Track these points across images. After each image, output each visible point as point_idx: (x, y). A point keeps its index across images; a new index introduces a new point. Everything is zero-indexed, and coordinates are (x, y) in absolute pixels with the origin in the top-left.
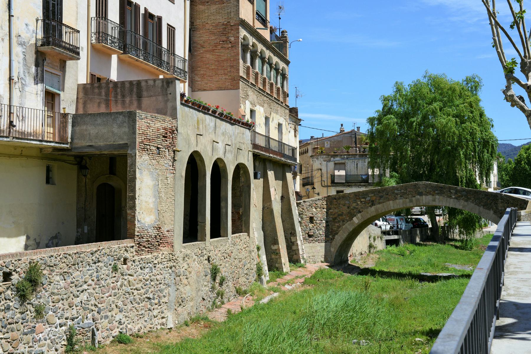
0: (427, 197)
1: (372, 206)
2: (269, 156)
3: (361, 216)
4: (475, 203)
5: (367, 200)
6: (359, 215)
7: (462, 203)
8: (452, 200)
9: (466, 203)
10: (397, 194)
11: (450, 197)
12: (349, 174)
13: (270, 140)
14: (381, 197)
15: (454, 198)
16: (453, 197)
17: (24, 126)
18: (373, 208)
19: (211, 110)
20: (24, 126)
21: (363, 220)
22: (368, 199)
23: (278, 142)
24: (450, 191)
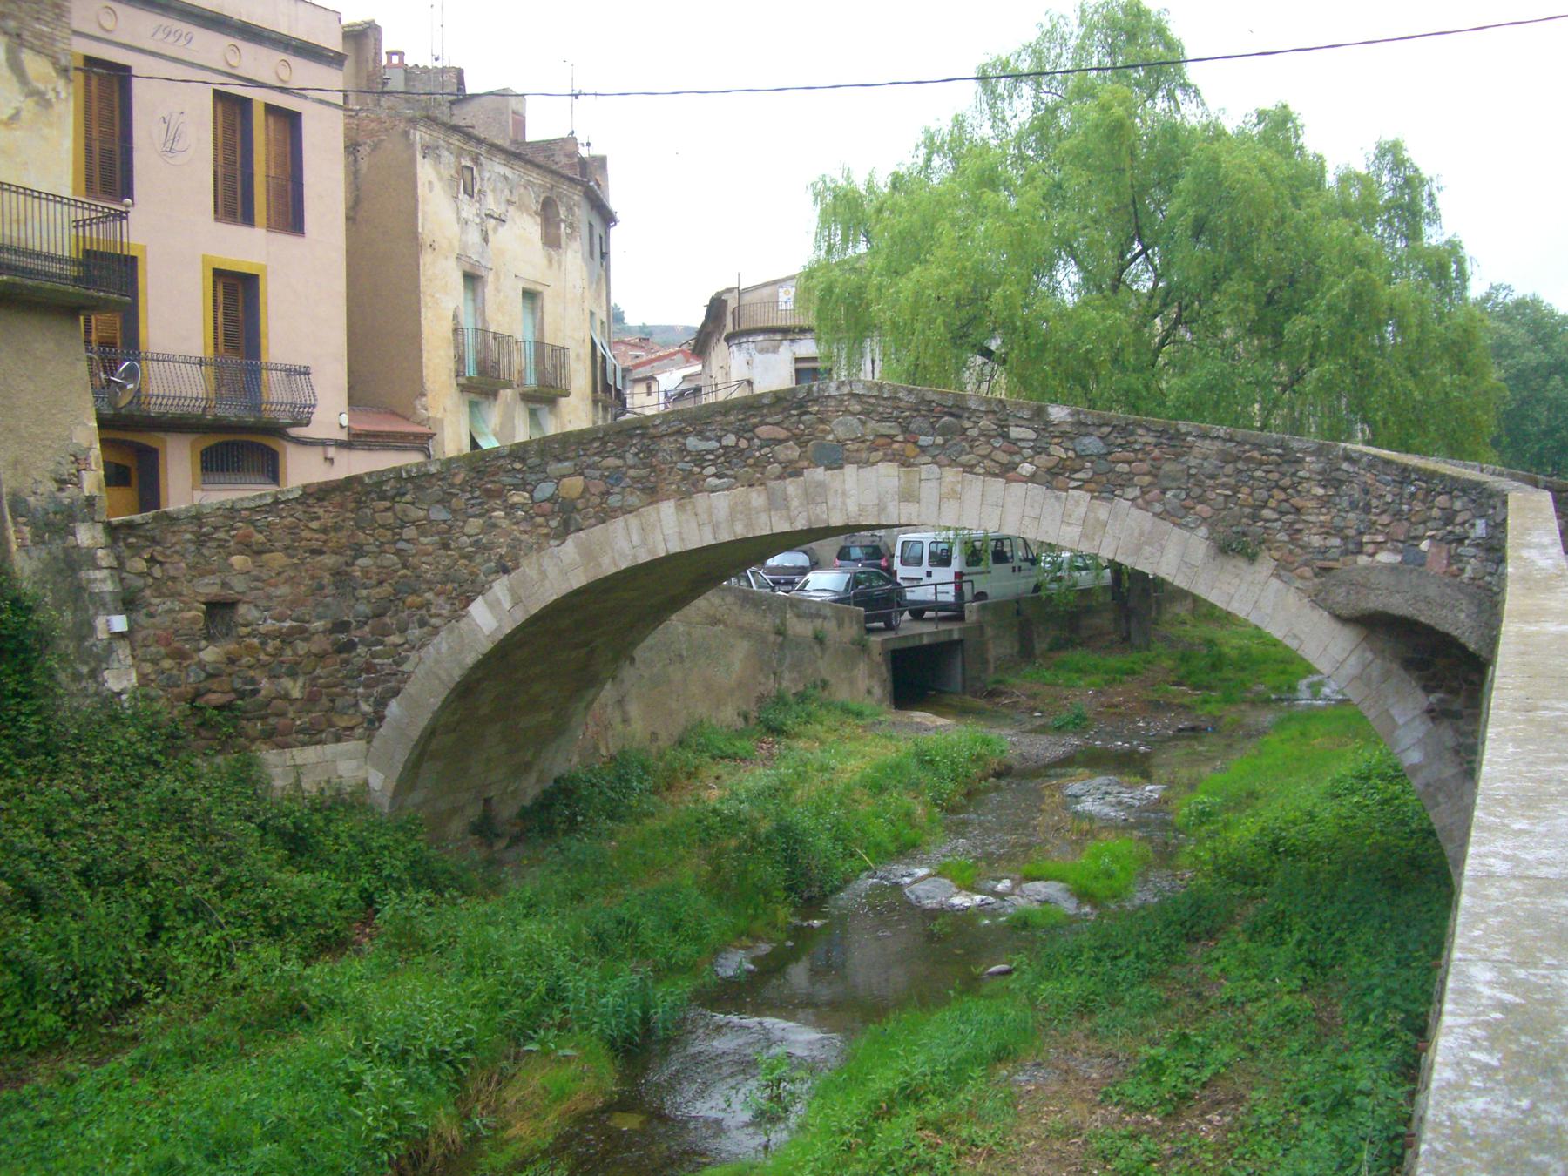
0: (869, 473)
1: (568, 533)
2: (87, 297)
3: (511, 590)
4: (1158, 508)
5: (538, 495)
6: (500, 588)
7: (1082, 510)
8: (1018, 489)
9: (1102, 511)
10: (700, 459)
11: (1006, 471)
12: (125, 253)
13: (341, 103)
14: (615, 477)
15: (1032, 479)
16: (1026, 469)
17: (51, 212)
18: (569, 549)
19: (796, 921)
20: (51, 212)
21: (520, 617)
22: (546, 490)
23: (976, 86)
24: (1005, 436)
